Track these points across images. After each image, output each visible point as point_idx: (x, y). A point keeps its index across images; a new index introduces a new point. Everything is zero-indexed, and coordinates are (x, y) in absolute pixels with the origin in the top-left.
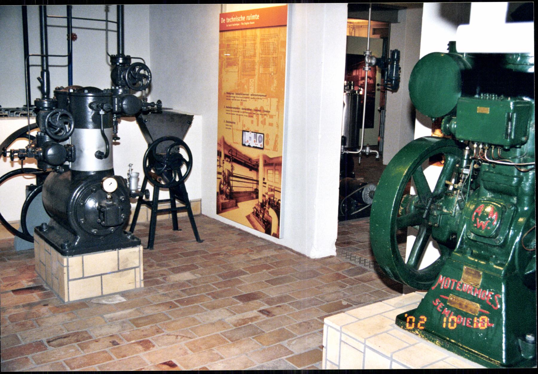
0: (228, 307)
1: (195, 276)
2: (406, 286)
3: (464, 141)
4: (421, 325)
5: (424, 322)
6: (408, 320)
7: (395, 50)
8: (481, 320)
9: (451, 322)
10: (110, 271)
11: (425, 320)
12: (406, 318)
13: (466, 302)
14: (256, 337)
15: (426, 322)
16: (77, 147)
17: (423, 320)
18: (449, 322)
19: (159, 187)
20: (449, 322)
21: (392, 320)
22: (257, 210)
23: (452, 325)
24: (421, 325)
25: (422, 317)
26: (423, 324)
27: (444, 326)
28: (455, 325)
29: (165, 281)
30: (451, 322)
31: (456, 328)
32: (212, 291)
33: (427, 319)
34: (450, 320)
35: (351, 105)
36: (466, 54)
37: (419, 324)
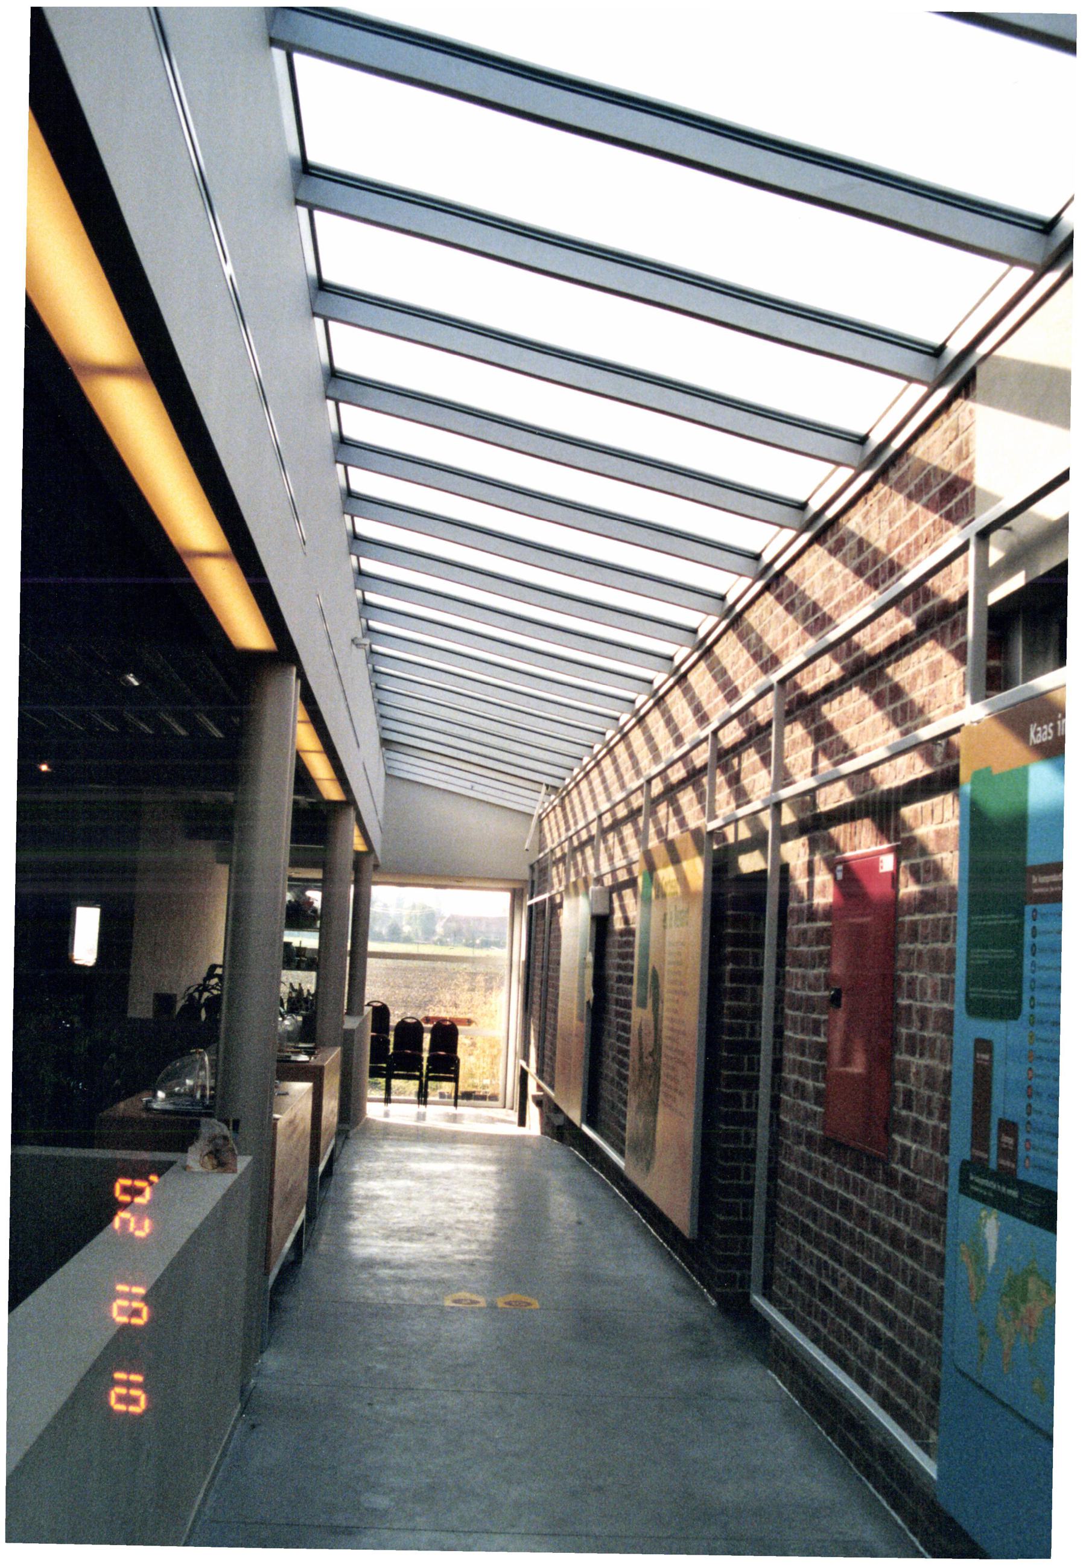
0: (917, 1206)
1: (811, 871)
5: (131, 1229)
6: (139, 1184)
8: (136, 1305)
14: (580, 1160)
15: (132, 1234)
17: (140, 1227)
20: (128, 1388)
23: (120, 1399)
25: (147, 1223)
27: (120, 1376)
32: (861, 1310)
33: (141, 1239)
34: (134, 1392)
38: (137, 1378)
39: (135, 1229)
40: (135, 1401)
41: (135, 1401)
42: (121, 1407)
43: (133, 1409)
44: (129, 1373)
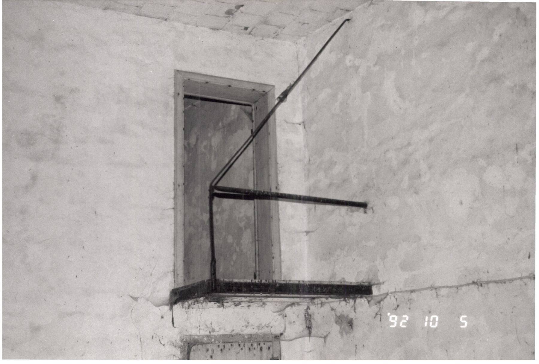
2: (361, 287)
4: (404, 324)
7: (210, 191)
9: (432, 321)
11: (407, 319)
12: (389, 316)
17: (405, 319)
19: (216, 280)
21: (352, 199)
23: (434, 324)
25: (404, 326)
28: (437, 324)
29: (283, 314)
30: (430, 321)
31: (461, 322)
34: (431, 319)
36: (184, 92)
37: (401, 323)
38: (427, 318)
40: (434, 319)
41: (434, 319)
43: (437, 320)
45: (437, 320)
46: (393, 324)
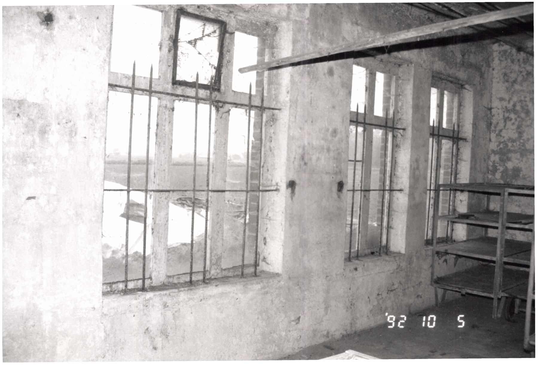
3: (334, 163)
4: (402, 324)
5: (404, 321)
9: (430, 321)
10: (247, 118)
11: (405, 319)
12: (387, 317)
13: (443, 155)
16: (209, 285)
17: (403, 319)
18: (428, 321)
22: (265, 330)
23: (431, 324)
24: (402, 324)
25: (402, 327)
26: (402, 320)
27: (424, 325)
34: (429, 319)
35: (439, 100)
37: (399, 323)
38: (424, 318)
39: (404, 320)
40: (432, 318)
41: (432, 318)
42: (434, 323)
43: (435, 319)
44: (422, 321)
45: (435, 319)
46: (391, 324)
